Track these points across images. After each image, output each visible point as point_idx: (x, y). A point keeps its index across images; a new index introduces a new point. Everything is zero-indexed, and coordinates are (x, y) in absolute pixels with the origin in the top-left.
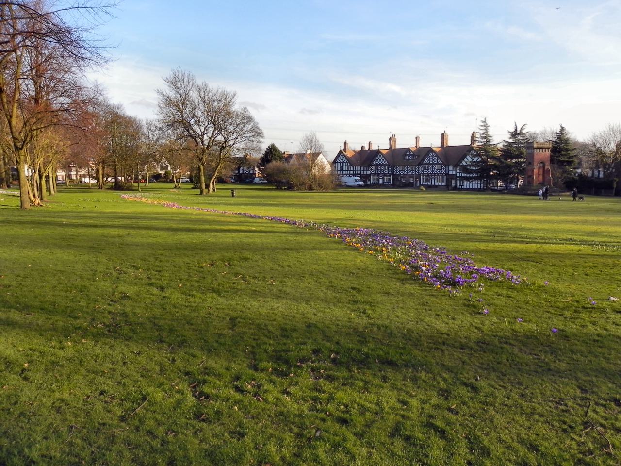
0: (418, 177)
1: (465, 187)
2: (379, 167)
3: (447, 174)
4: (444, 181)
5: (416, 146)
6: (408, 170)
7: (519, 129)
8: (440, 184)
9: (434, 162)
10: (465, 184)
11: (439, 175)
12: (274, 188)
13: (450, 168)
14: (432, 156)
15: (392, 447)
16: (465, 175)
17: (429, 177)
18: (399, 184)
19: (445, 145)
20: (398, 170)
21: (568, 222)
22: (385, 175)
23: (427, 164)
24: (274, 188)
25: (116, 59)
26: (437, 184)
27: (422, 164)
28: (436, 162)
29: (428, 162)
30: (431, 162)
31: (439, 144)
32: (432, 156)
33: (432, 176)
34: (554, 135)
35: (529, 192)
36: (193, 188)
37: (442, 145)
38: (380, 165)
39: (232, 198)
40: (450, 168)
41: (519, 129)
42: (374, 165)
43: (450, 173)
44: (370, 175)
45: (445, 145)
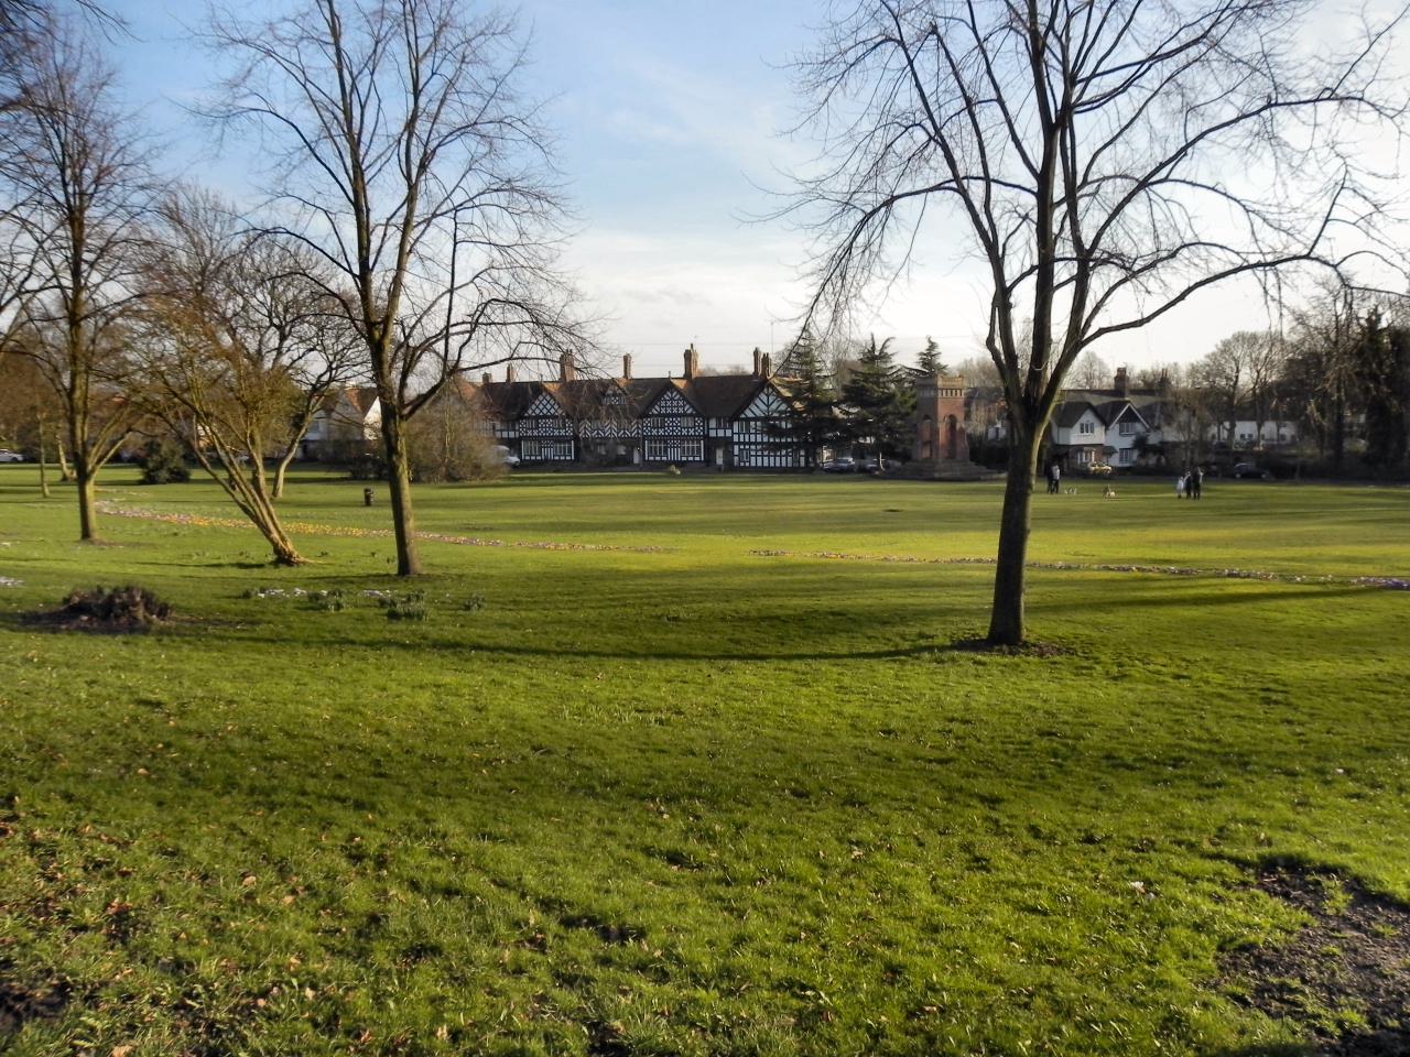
0: (632, 444)
1: (753, 464)
2: (541, 422)
3: (706, 437)
4: (699, 451)
5: (626, 376)
6: (610, 429)
7: (878, 348)
8: (691, 459)
9: (675, 411)
10: (753, 459)
11: (688, 438)
12: (345, 475)
13: (713, 424)
14: (672, 399)
15: (326, 921)
16: (765, 440)
17: (665, 442)
18: (593, 460)
19: (694, 375)
20: (587, 430)
21: (1205, 543)
22: (559, 440)
23: (659, 415)
24: (345, 475)
25: (1378, 236)
26: (684, 459)
27: (648, 416)
28: (681, 410)
29: (663, 411)
30: (669, 411)
31: (680, 372)
32: (672, 399)
33: (670, 443)
34: (917, 358)
35: (936, 475)
36: (141, 483)
37: (687, 376)
38: (545, 417)
39: (369, 510)
40: (713, 424)
41: (878, 348)
42: (530, 417)
43: (713, 434)
44: (520, 438)
45: (694, 375)
